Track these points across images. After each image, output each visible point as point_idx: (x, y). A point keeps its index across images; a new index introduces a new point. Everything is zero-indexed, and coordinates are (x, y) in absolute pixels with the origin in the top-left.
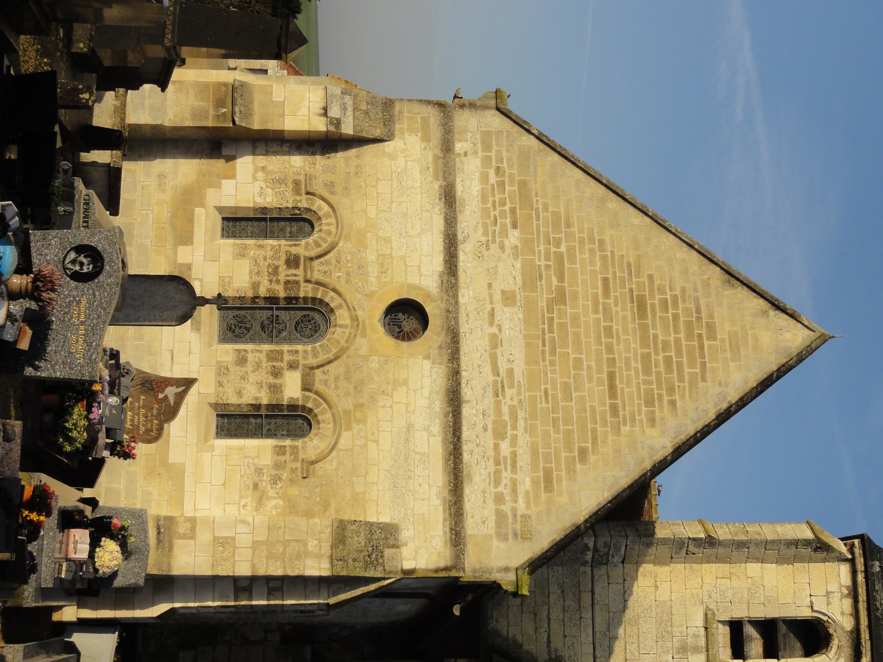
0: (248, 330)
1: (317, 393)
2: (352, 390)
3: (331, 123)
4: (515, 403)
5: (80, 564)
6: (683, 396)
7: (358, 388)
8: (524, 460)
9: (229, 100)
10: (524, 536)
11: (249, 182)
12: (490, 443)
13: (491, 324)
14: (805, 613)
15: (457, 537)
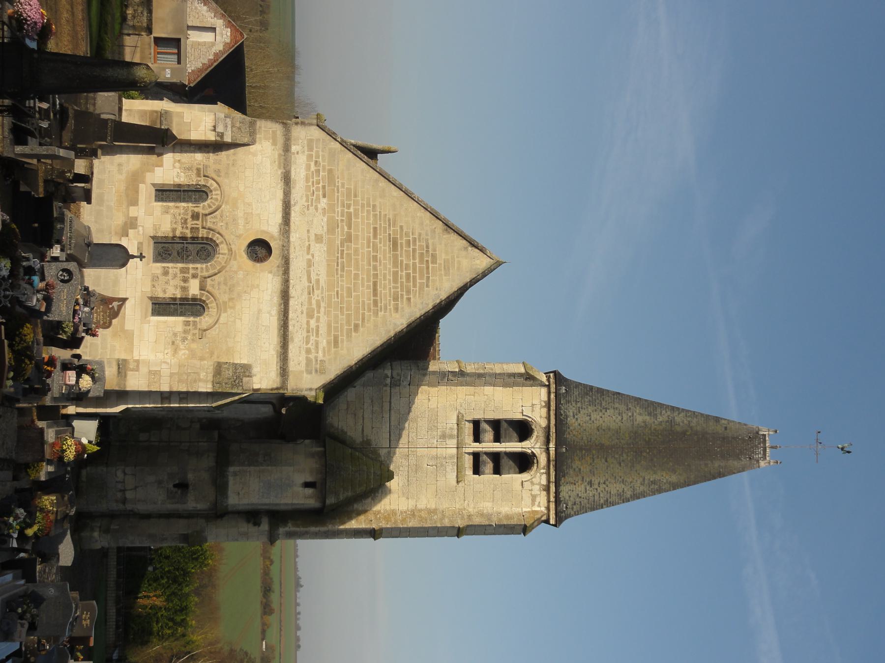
0: (170, 255)
1: (208, 292)
2: (227, 290)
5: (71, 386)
6: (415, 296)
7: (231, 290)
8: (323, 330)
10: (321, 371)
11: (170, 168)
12: (305, 320)
13: (308, 254)
14: (519, 416)
15: (284, 372)
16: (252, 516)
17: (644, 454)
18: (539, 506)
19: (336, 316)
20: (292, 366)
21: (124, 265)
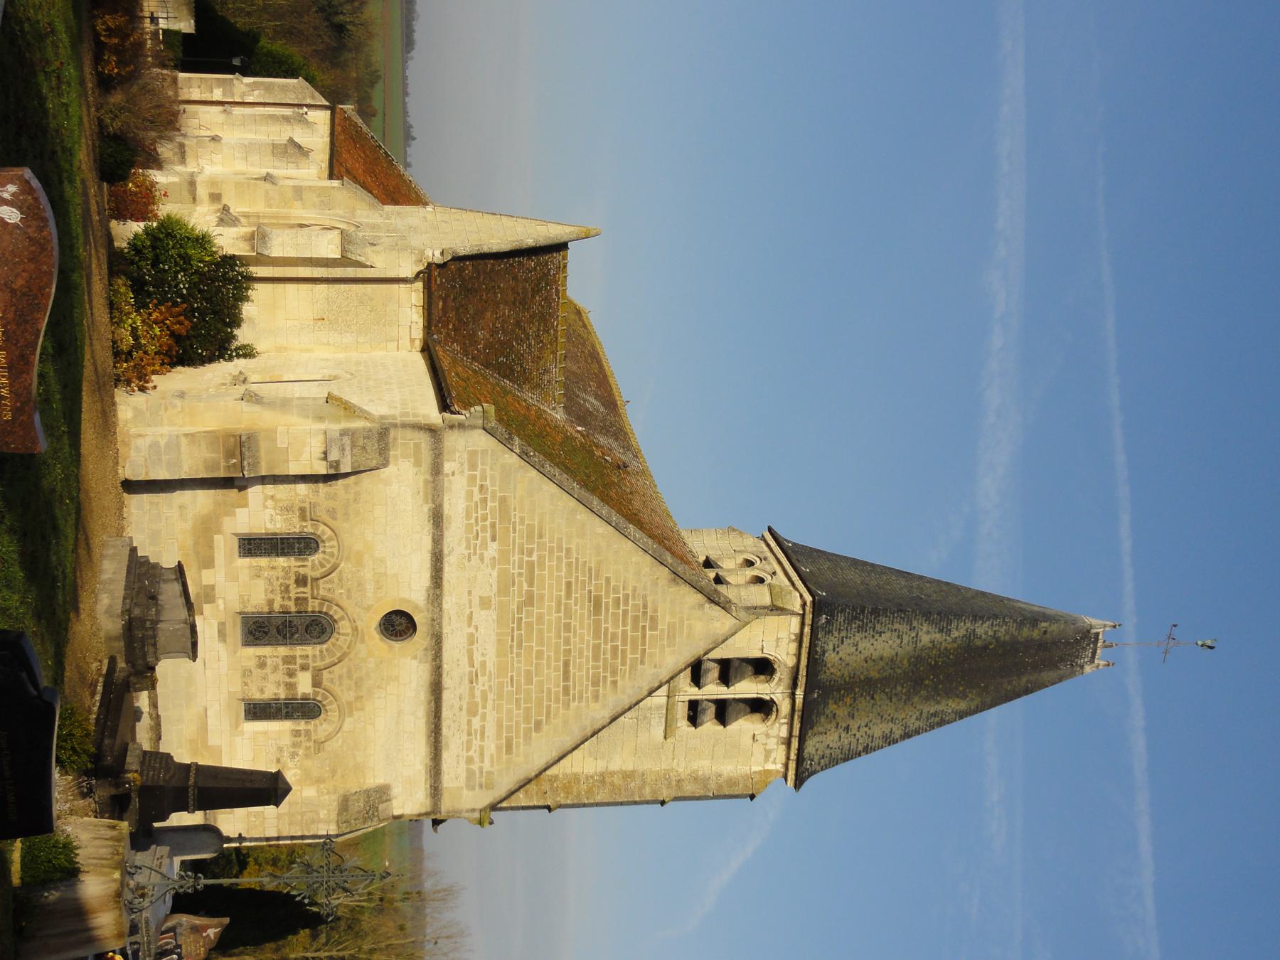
0: (266, 633)
3: (331, 467)
7: (358, 684)
8: (491, 730)
9: (238, 452)
13: (469, 625)
14: (758, 654)
15: (435, 791)
18: (774, 762)
20: (447, 781)
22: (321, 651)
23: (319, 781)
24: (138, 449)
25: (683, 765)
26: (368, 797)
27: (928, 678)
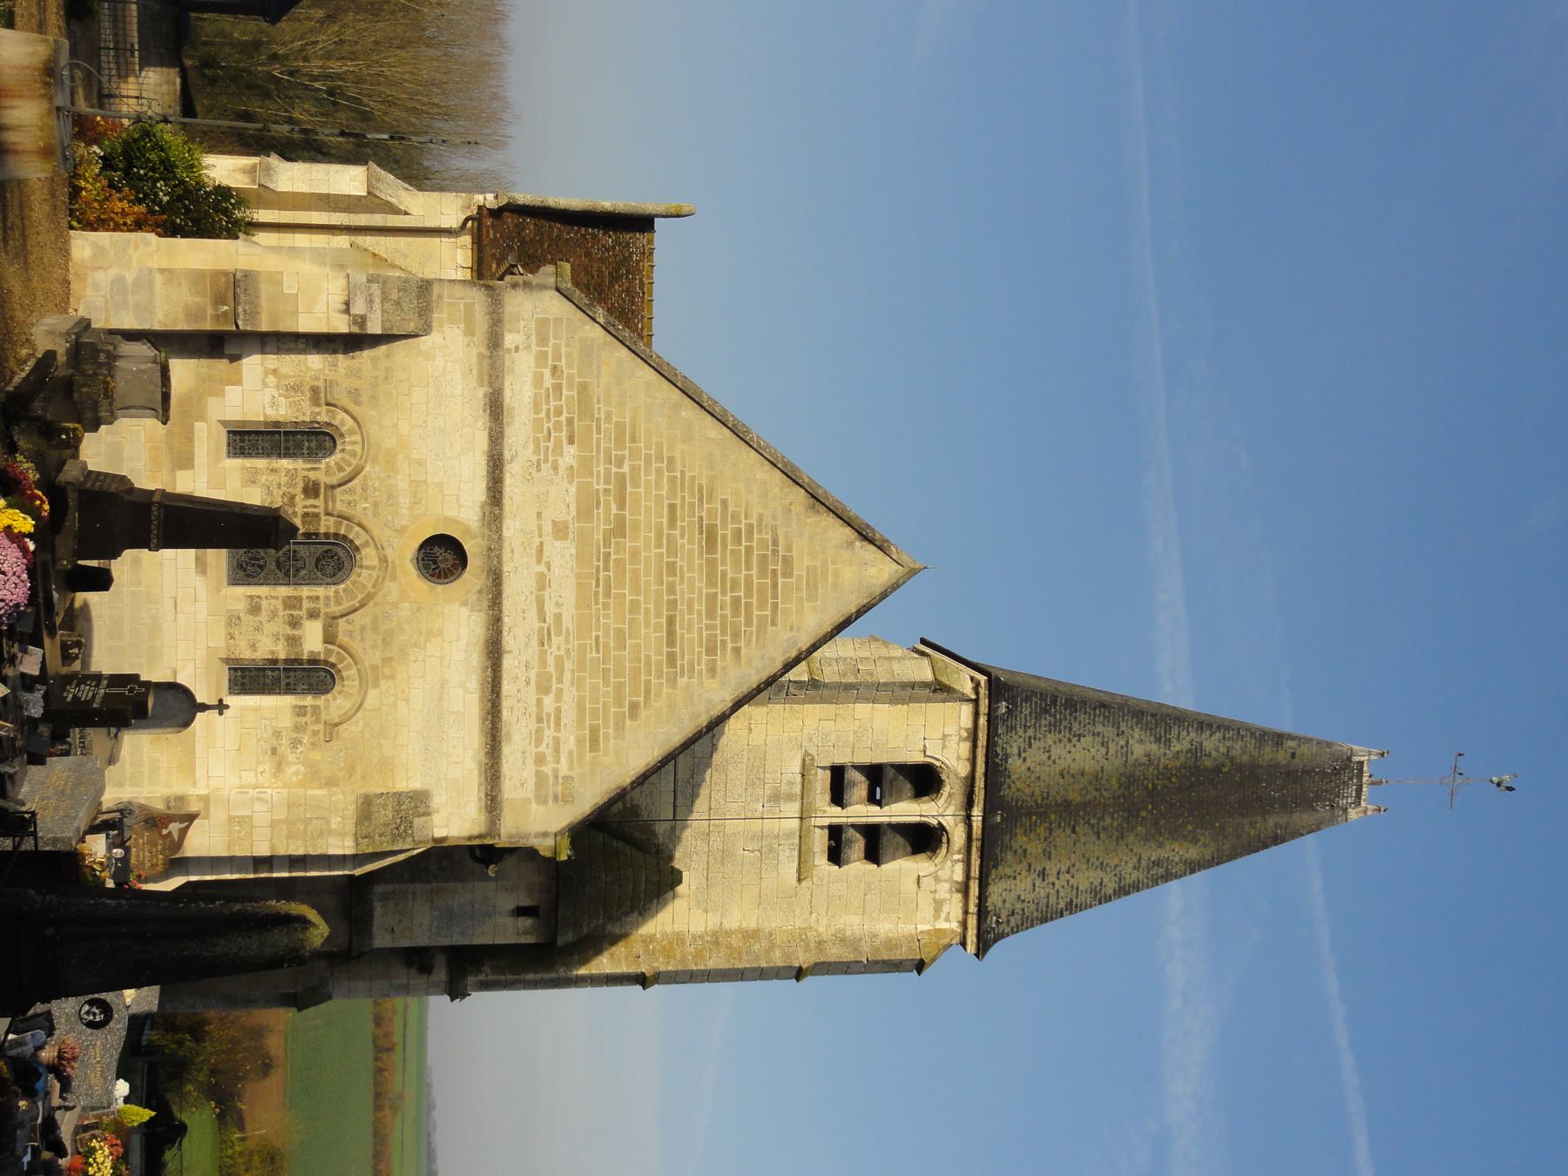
0: (261, 567)
4: (562, 652)
7: (388, 638)
8: (569, 716)
9: (231, 295)
10: (565, 798)
13: (539, 561)
14: (918, 758)
15: (493, 803)
16: (418, 960)
17: (1144, 814)
18: (947, 919)
19: (595, 688)
21: (187, 724)
22: (337, 592)
23: (331, 783)
24: (97, 287)
25: (824, 922)
26: (400, 804)
27: (1145, 808)
